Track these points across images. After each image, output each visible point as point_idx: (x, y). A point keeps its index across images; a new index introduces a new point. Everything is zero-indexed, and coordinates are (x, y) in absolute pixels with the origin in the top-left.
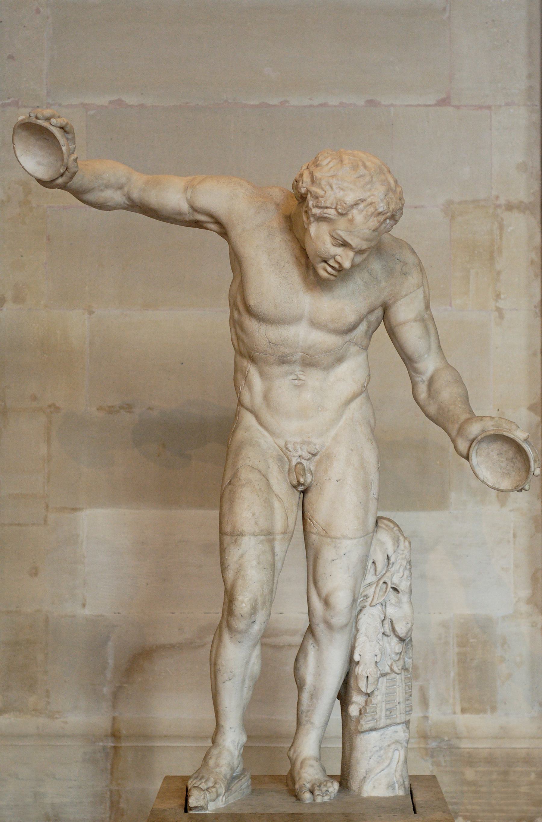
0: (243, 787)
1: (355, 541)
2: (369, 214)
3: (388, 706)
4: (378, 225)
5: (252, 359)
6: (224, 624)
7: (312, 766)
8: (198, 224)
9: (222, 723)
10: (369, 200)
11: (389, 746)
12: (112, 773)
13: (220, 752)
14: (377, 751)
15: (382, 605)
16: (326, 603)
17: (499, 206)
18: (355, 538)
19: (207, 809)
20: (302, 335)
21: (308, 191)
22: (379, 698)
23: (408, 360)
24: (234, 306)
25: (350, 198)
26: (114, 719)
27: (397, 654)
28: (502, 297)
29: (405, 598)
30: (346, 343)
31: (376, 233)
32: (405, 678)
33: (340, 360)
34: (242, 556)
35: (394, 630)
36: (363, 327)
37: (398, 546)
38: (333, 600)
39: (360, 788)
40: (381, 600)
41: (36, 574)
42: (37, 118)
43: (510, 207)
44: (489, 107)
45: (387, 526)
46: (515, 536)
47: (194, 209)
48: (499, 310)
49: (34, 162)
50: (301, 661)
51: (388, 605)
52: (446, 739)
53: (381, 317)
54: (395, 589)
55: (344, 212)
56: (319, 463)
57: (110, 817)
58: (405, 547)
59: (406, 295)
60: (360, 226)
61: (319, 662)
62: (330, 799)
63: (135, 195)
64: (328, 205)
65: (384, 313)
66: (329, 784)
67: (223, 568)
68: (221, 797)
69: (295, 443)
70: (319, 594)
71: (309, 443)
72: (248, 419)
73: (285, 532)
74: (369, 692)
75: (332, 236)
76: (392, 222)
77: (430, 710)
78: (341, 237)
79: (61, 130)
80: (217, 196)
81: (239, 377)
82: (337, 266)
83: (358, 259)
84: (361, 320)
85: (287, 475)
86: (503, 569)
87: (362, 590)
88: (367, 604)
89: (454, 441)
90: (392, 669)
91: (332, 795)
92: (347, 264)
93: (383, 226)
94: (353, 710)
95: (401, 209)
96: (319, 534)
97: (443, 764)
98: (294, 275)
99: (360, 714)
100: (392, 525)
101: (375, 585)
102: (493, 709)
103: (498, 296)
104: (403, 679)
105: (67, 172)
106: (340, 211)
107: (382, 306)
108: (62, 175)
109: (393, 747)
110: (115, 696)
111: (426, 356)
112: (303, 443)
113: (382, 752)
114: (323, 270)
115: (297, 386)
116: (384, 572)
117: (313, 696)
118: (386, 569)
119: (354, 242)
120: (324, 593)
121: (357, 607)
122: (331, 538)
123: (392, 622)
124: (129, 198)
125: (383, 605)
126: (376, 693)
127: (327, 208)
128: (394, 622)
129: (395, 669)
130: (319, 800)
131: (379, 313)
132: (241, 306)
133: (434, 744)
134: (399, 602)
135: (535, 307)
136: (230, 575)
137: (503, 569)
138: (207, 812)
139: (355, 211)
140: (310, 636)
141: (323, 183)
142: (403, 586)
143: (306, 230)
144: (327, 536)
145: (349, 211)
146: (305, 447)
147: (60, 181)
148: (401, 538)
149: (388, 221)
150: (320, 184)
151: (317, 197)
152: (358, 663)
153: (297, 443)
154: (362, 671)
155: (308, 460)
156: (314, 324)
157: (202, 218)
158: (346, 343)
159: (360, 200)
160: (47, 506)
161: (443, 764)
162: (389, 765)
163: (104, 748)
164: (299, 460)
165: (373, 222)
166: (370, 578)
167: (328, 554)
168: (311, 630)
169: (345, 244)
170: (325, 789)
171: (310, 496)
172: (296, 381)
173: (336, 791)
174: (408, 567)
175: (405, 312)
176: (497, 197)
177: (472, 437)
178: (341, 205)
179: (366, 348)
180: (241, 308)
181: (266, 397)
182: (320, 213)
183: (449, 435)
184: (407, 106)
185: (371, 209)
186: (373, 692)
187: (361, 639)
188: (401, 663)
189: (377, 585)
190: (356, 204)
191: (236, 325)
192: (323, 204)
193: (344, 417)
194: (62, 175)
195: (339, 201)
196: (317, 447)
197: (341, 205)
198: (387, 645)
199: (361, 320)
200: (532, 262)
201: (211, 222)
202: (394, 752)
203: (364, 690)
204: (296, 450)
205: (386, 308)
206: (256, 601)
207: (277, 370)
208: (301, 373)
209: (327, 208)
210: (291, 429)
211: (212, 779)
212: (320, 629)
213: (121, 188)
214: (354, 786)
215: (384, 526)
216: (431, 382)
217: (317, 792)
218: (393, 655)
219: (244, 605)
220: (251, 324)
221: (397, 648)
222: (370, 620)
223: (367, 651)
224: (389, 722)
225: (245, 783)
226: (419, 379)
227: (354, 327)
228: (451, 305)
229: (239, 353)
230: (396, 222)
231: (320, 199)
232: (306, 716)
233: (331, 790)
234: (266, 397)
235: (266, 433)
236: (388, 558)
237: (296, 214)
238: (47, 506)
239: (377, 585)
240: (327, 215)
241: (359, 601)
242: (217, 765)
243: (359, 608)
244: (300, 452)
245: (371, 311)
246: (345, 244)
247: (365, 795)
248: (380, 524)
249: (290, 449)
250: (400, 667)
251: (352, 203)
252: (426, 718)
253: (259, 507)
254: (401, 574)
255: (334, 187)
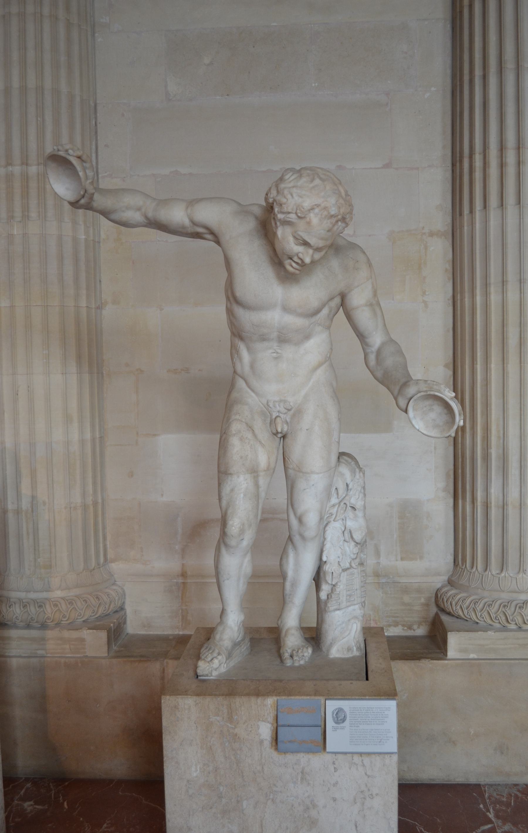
0: (243, 650)
1: (321, 475)
2: (323, 216)
3: (348, 593)
4: (331, 226)
5: (241, 338)
6: (221, 541)
7: (293, 635)
8: (197, 236)
9: (225, 608)
10: (323, 205)
11: (349, 620)
12: (182, 599)
13: (224, 629)
14: (340, 624)
15: (343, 520)
16: (300, 520)
17: (424, 234)
18: (321, 473)
19: (212, 676)
20: (275, 317)
21: (274, 200)
22: (341, 587)
23: (361, 336)
24: (228, 298)
25: (307, 204)
26: (183, 564)
27: (354, 554)
28: (427, 293)
29: (360, 514)
30: (312, 324)
31: (330, 234)
32: (361, 571)
33: (307, 337)
34: (232, 490)
35: (352, 537)
36: (325, 311)
37: (355, 476)
38: (305, 519)
39: (328, 651)
40: (343, 517)
41: (132, 476)
42: (58, 150)
43: (431, 234)
44: (417, 169)
45: (346, 461)
46: (435, 448)
47: (194, 223)
48: (425, 302)
49: (62, 187)
50: (284, 561)
51: (347, 520)
52: (391, 577)
53: (340, 304)
54: (353, 508)
55: (303, 216)
56: (294, 415)
57: (182, 625)
58: (360, 477)
59: (358, 286)
60: (317, 228)
61: (297, 563)
62: (305, 662)
63: (150, 215)
64: (290, 211)
65: (342, 301)
66: (305, 649)
67: (220, 499)
68: (223, 665)
69: (274, 402)
70: (295, 514)
71: (285, 401)
72: (241, 383)
73: (268, 469)
74: (333, 583)
75: (294, 237)
76: (344, 225)
77: (381, 558)
78: (301, 237)
79: (79, 160)
80: (208, 214)
81: (234, 351)
82: (300, 262)
83: (317, 256)
84: (324, 306)
85: (268, 425)
86: (427, 469)
87: (327, 509)
88: (332, 519)
89: (396, 399)
90: (351, 566)
91: (307, 659)
92: (308, 260)
93: (336, 227)
94: (323, 595)
95: (351, 213)
96: (294, 469)
97: (389, 592)
98: (269, 272)
99: (328, 598)
100: (350, 460)
101: (337, 506)
102: (421, 558)
103: (424, 293)
104: (359, 572)
105: (86, 194)
106: (299, 215)
107: (339, 294)
108: (83, 197)
109: (352, 621)
110: (183, 550)
111: (374, 333)
112: (281, 401)
113: (344, 625)
114: (290, 267)
115: (276, 358)
116: (344, 496)
117: (294, 585)
118: (345, 493)
119: (313, 241)
120: (299, 511)
121: (324, 524)
122: (303, 473)
123: (350, 532)
124: (146, 217)
125: (344, 520)
126: (339, 584)
127: (289, 213)
128: (352, 532)
129: (353, 565)
130: (297, 664)
131: (338, 300)
132: (232, 299)
133: (384, 580)
134: (356, 516)
135: (448, 300)
136: (224, 503)
137: (427, 469)
138: (212, 678)
139: (312, 215)
140: (290, 543)
141: (286, 192)
142: (359, 504)
143: (275, 234)
144: (300, 471)
145: (306, 214)
146: (282, 404)
147: (83, 201)
148: (357, 470)
149: (340, 223)
150: (283, 193)
151: (281, 205)
152: (325, 562)
153: (276, 402)
154: (329, 568)
155: (285, 414)
156: (286, 309)
157: (200, 230)
158: (312, 324)
159: (316, 205)
160: (137, 433)
161: (389, 592)
162: (349, 634)
163: (177, 583)
164: (278, 414)
165: (327, 224)
166: (334, 500)
167: (301, 484)
168: (290, 538)
169: (306, 244)
170: (302, 654)
171: (288, 440)
172: (275, 354)
173: (310, 654)
174: (363, 491)
175: (359, 299)
176: (423, 228)
177: (409, 396)
178: (300, 210)
179: (328, 328)
180: (231, 299)
181: (252, 366)
182: (284, 218)
183: (392, 394)
184: (363, 169)
185: (325, 213)
186: (337, 583)
187: (328, 546)
188: (358, 561)
189: (339, 506)
190: (312, 209)
191: (230, 312)
192: (285, 210)
193: (312, 381)
194: (83, 197)
195: (299, 207)
196: (291, 404)
197: (300, 210)
198: (347, 548)
199: (324, 306)
200: (446, 270)
201: (208, 234)
202: (353, 624)
203: (330, 582)
204: (275, 406)
205: (343, 297)
206: (243, 525)
207: (259, 346)
208: (278, 348)
209: (289, 213)
210: (271, 390)
211: (217, 651)
212: (297, 538)
213: (139, 209)
214: (324, 649)
215: (344, 461)
216: (379, 352)
217: (295, 658)
218: (352, 555)
219: (234, 528)
220: (239, 312)
221: (354, 550)
222: (334, 531)
223: (331, 555)
224: (348, 604)
225: (245, 648)
226: (370, 350)
227: (318, 311)
228: (393, 300)
229: (233, 334)
230: (347, 225)
231: (283, 206)
232: (289, 598)
233: (306, 654)
234: (252, 366)
235: (253, 394)
236: (347, 485)
237: (267, 223)
238: (137, 433)
239: (339, 506)
240: (290, 219)
241: (325, 517)
242: (221, 639)
243: (325, 522)
244: (278, 408)
245: (331, 299)
246: (306, 244)
247: (331, 656)
248: (341, 460)
249: (271, 406)
250: (357, 564)
251: (309, 208)
252: (378, 563)
253: (250, 449)
254: (357, 497)
255: (294, 195)
